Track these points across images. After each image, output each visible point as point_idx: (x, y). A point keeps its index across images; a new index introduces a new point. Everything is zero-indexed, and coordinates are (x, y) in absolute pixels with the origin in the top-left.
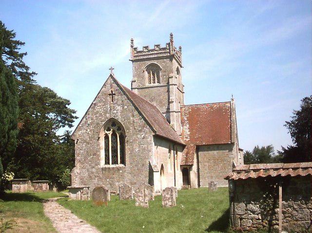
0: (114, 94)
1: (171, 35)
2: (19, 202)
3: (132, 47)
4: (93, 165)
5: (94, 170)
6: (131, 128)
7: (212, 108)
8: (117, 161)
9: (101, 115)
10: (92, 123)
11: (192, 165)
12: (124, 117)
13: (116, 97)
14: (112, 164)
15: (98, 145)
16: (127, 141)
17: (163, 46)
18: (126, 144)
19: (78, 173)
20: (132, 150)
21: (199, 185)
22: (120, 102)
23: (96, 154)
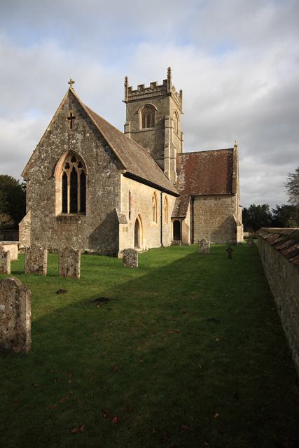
2: (227, 182)
3: (126, 86)
4: (47, 212)
5: (48, 220)
6: (94, 164)
7: (212, 155)
8: (77, 209)
9: (57, 147)
10: (46, 159)
11: (184, 218)
12: (85, 149)
13: (76, 121)
14: (71, 212)
15: (54, 186)
16: (89, 181)
18: (87, 185)
19: (28, 223)
20: (94, 194)
21: (192, 241)
22: (81, 128)
23: (51, 199)
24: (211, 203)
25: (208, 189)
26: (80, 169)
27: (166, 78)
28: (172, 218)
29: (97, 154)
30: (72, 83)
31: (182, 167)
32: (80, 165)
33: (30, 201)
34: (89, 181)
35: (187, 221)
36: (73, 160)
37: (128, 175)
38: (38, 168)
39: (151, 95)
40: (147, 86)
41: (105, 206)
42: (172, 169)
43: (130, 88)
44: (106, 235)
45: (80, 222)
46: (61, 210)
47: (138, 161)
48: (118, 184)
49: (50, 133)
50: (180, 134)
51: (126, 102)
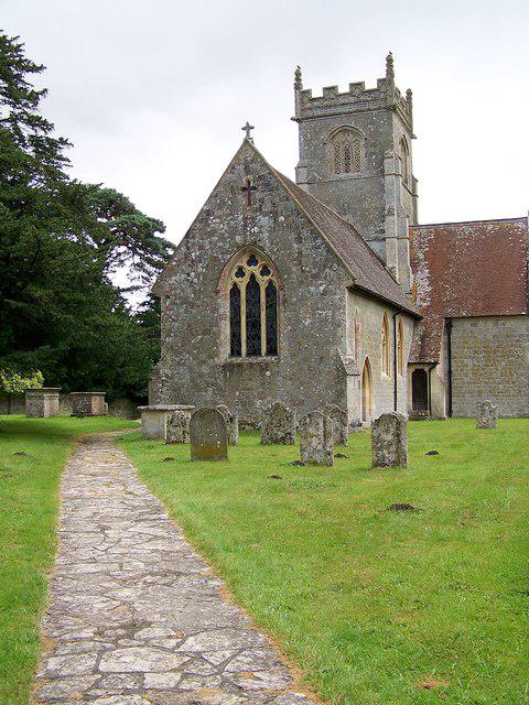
0: (254, 188)
1: (390, 60)
3: (298, 86)
4: (203, 356)
5: (205, 369)
6: (294, 269)
7: (483, 231)
9: (222, 238)
11: (436, 363)
13: (258, 195)
14: (248, 354)
17: (371, 85)
23: (210, 330)
24: (488, 329)
25: (480, 304)
26: (266, 278)
27: (384, 76)
28: (409, 364)
29: (300, 253)
30: (248, 128)
31: (421, 256)
32: (265, 271)
33: (168, 336)
34: (285, 301)
35: (439, 372)
36: (253, 261)
37: (358, 291)
38: (184, 276)
39: (354, 108)
40: (344, 89)
41: (318, 344)
42: (402, 260)
43: (308, 92)
44: (320, 395)
45: (268, 373)
46: (229, 351)
47: (344, 245)
48: (338, 307)
49: (209, 215)
50: (410, 182)
51: (297, 120)
